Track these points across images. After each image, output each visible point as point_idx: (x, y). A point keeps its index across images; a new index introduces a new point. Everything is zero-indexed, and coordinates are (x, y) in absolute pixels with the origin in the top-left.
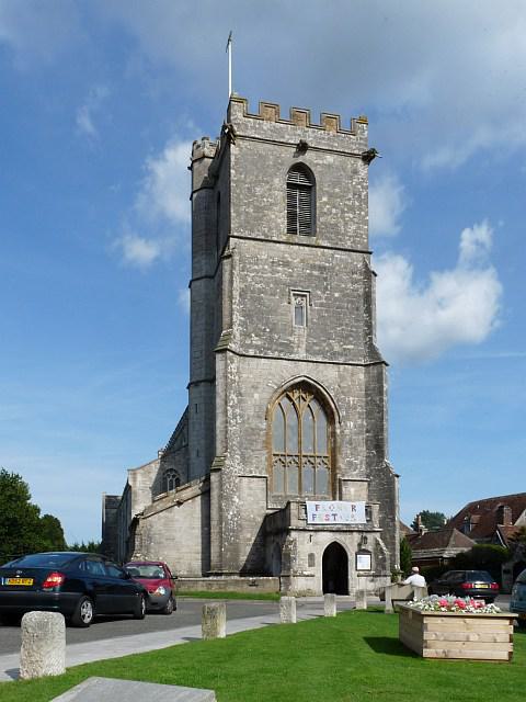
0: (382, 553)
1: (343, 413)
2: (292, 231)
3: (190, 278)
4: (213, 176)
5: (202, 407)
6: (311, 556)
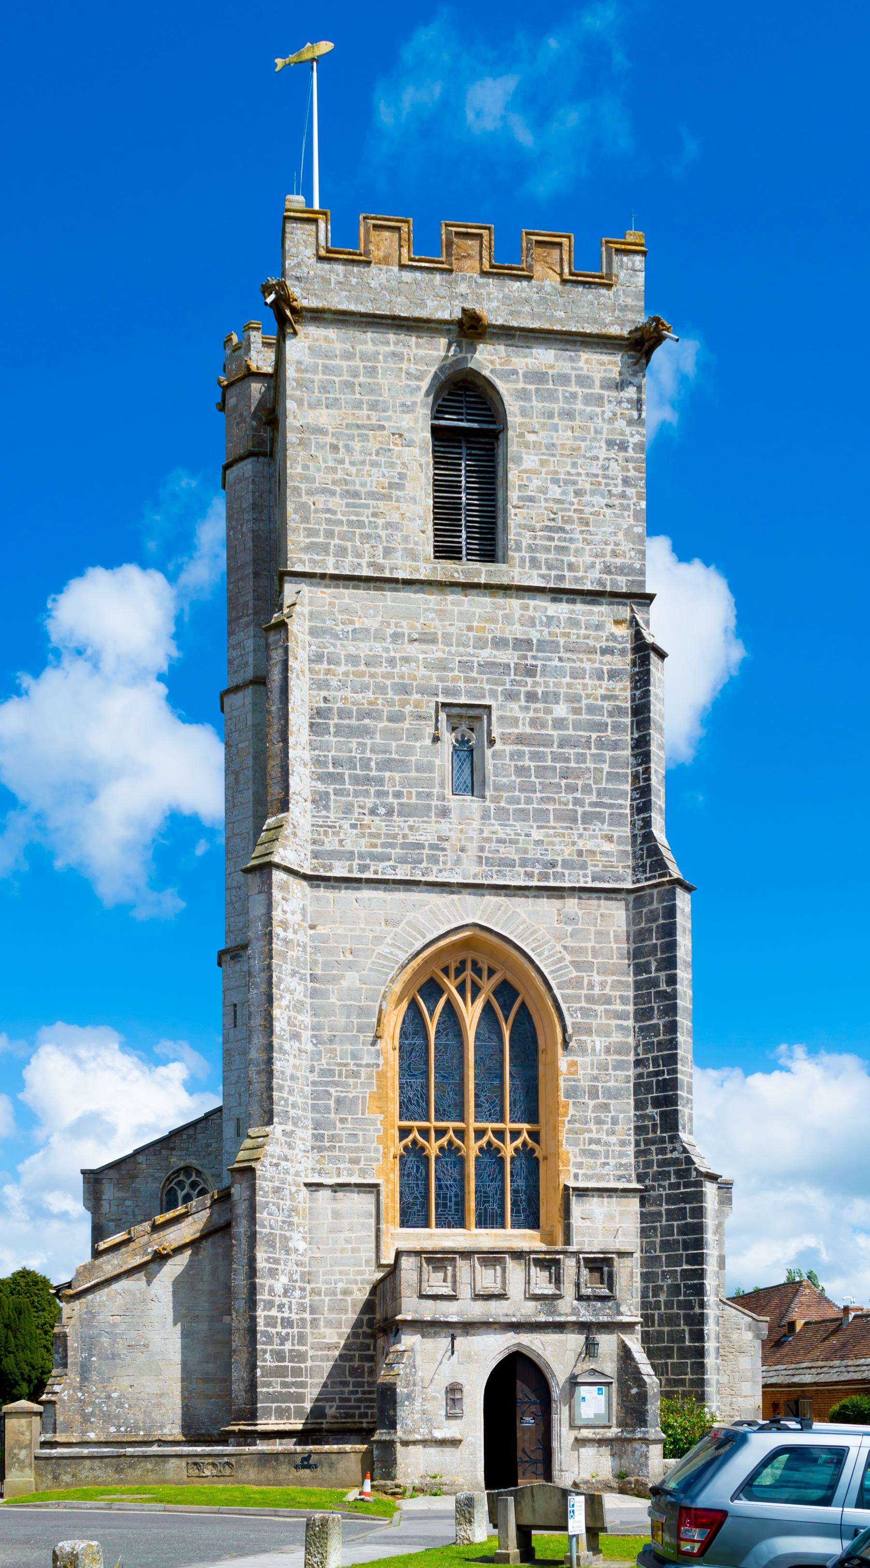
6: (454, 1392)
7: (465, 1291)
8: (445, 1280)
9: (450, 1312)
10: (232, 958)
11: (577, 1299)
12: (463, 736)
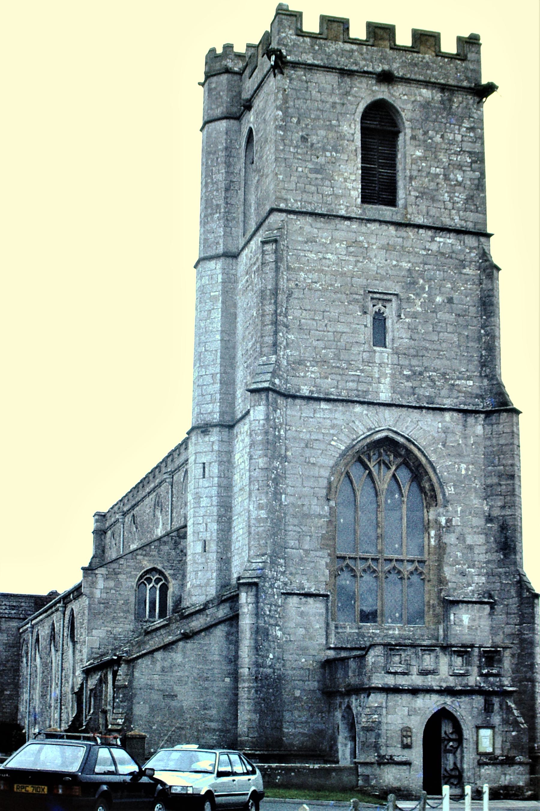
1: (450, 490)
2: (367, 198)
3: (190, 427)
4: (230, 662)
5: (215, 469)
7: (414, 670)
8: (455, 675)
9: (403, 681)
10: (202, 432)
11: (479, 676)
12: (379, 310)
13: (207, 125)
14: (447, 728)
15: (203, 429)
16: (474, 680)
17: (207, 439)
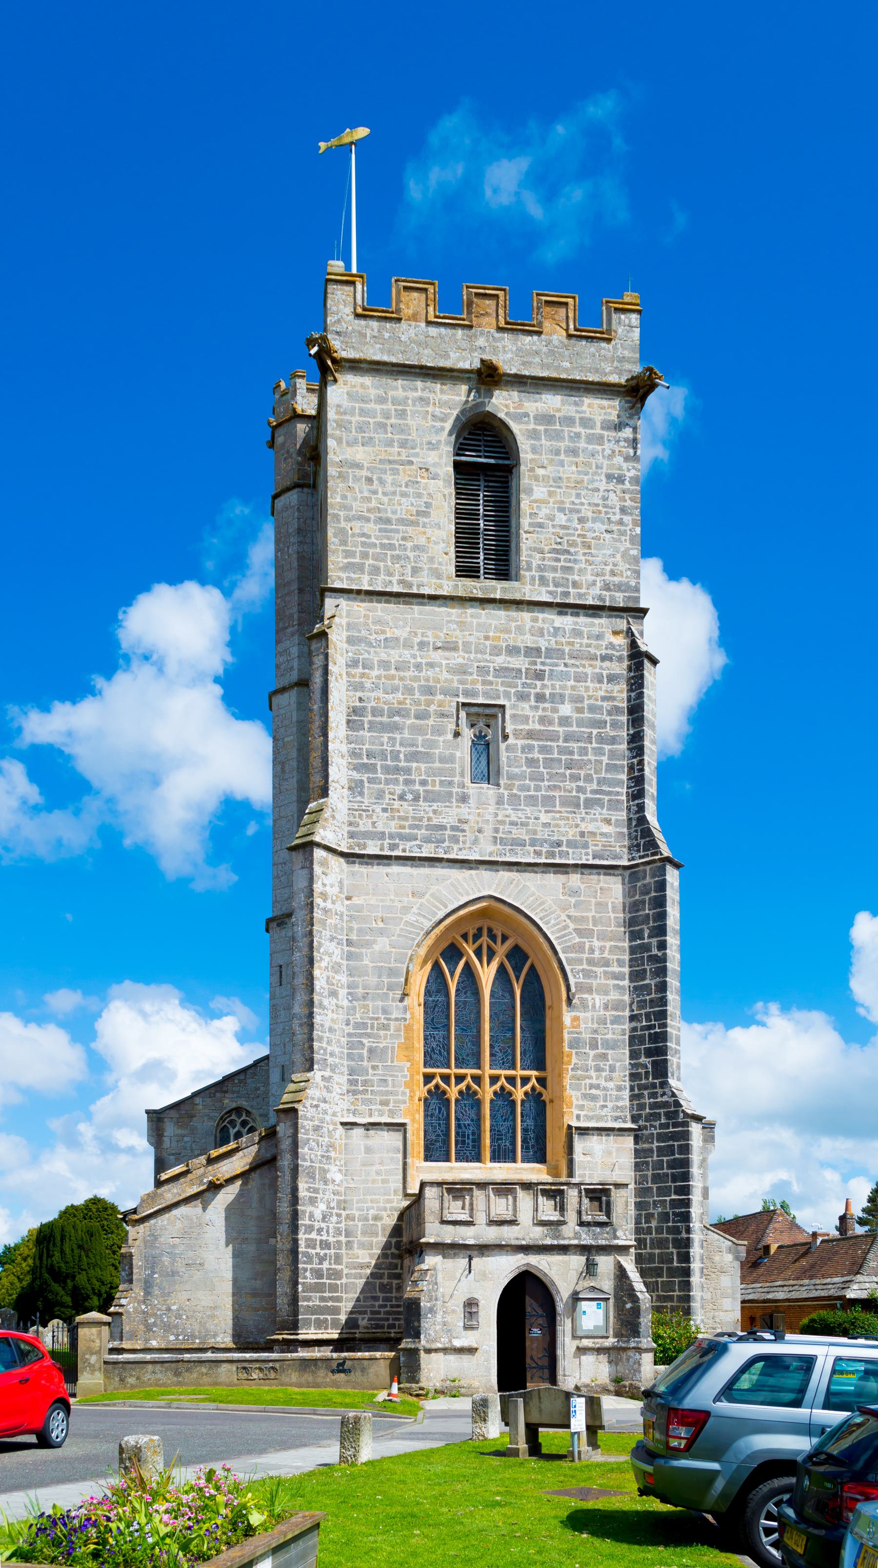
0: (634, 1299)
2: (466, 571)
6: (471, 1306)
10: (278, 925)
11: (579, 1225)
12: (480, 732)
13: (276, 501)
14: (531, 1305)
15: (280, 921)
16: (571, 1233)
17: (283, 933)
